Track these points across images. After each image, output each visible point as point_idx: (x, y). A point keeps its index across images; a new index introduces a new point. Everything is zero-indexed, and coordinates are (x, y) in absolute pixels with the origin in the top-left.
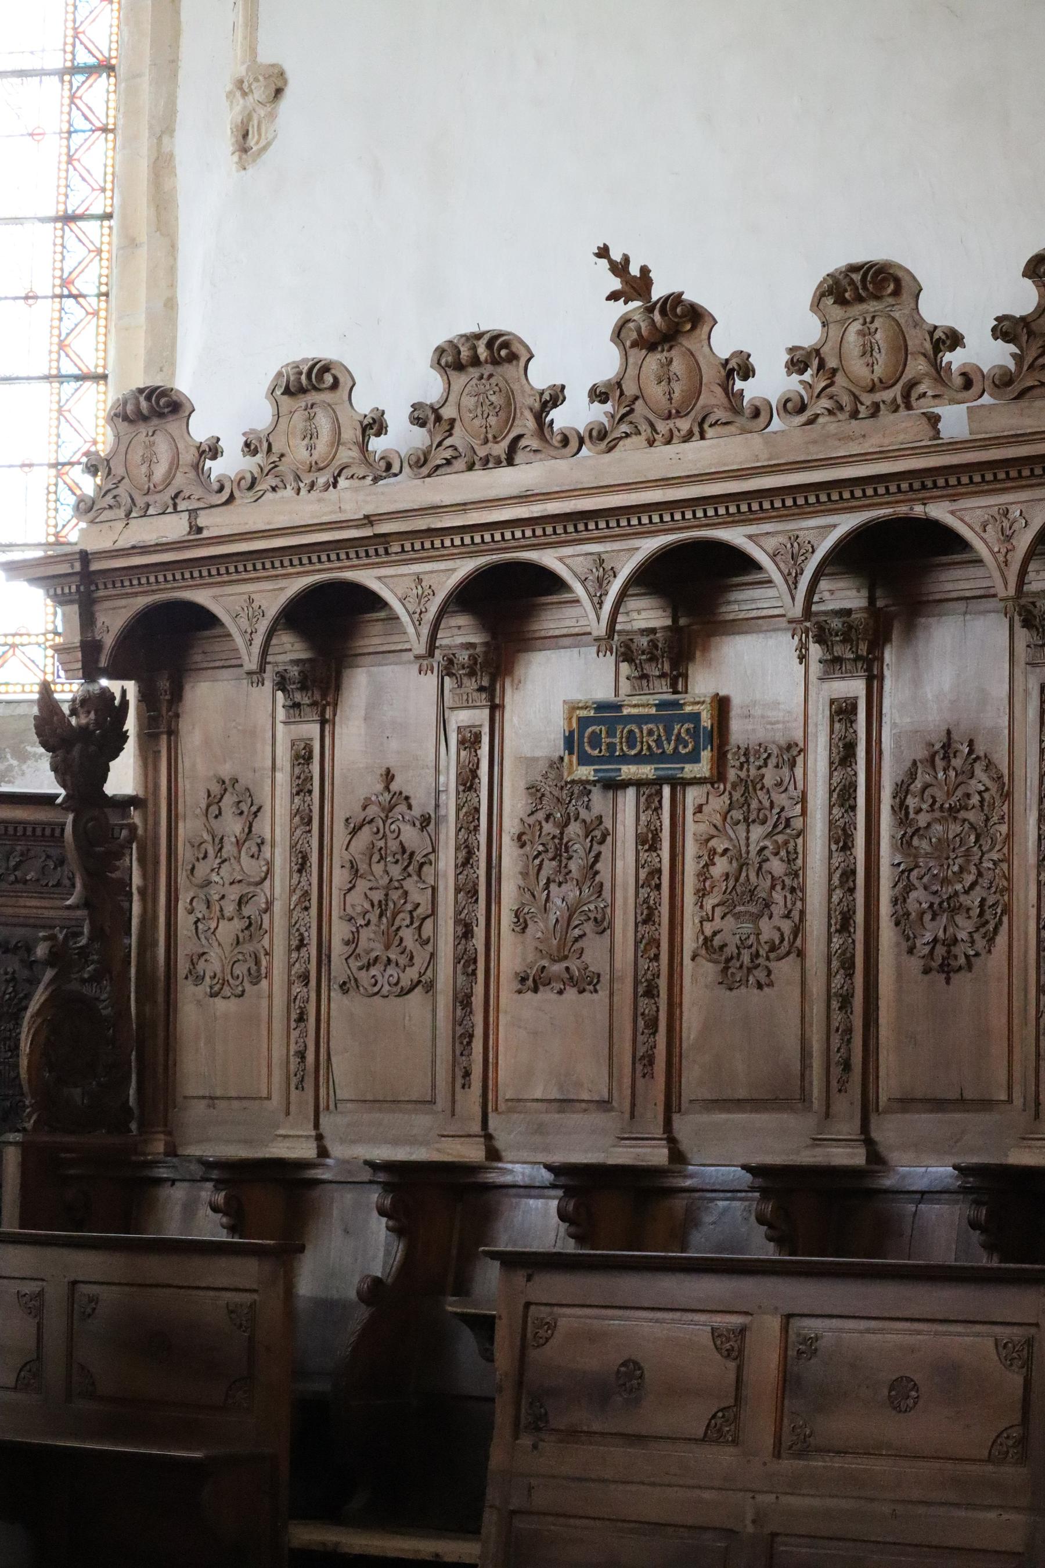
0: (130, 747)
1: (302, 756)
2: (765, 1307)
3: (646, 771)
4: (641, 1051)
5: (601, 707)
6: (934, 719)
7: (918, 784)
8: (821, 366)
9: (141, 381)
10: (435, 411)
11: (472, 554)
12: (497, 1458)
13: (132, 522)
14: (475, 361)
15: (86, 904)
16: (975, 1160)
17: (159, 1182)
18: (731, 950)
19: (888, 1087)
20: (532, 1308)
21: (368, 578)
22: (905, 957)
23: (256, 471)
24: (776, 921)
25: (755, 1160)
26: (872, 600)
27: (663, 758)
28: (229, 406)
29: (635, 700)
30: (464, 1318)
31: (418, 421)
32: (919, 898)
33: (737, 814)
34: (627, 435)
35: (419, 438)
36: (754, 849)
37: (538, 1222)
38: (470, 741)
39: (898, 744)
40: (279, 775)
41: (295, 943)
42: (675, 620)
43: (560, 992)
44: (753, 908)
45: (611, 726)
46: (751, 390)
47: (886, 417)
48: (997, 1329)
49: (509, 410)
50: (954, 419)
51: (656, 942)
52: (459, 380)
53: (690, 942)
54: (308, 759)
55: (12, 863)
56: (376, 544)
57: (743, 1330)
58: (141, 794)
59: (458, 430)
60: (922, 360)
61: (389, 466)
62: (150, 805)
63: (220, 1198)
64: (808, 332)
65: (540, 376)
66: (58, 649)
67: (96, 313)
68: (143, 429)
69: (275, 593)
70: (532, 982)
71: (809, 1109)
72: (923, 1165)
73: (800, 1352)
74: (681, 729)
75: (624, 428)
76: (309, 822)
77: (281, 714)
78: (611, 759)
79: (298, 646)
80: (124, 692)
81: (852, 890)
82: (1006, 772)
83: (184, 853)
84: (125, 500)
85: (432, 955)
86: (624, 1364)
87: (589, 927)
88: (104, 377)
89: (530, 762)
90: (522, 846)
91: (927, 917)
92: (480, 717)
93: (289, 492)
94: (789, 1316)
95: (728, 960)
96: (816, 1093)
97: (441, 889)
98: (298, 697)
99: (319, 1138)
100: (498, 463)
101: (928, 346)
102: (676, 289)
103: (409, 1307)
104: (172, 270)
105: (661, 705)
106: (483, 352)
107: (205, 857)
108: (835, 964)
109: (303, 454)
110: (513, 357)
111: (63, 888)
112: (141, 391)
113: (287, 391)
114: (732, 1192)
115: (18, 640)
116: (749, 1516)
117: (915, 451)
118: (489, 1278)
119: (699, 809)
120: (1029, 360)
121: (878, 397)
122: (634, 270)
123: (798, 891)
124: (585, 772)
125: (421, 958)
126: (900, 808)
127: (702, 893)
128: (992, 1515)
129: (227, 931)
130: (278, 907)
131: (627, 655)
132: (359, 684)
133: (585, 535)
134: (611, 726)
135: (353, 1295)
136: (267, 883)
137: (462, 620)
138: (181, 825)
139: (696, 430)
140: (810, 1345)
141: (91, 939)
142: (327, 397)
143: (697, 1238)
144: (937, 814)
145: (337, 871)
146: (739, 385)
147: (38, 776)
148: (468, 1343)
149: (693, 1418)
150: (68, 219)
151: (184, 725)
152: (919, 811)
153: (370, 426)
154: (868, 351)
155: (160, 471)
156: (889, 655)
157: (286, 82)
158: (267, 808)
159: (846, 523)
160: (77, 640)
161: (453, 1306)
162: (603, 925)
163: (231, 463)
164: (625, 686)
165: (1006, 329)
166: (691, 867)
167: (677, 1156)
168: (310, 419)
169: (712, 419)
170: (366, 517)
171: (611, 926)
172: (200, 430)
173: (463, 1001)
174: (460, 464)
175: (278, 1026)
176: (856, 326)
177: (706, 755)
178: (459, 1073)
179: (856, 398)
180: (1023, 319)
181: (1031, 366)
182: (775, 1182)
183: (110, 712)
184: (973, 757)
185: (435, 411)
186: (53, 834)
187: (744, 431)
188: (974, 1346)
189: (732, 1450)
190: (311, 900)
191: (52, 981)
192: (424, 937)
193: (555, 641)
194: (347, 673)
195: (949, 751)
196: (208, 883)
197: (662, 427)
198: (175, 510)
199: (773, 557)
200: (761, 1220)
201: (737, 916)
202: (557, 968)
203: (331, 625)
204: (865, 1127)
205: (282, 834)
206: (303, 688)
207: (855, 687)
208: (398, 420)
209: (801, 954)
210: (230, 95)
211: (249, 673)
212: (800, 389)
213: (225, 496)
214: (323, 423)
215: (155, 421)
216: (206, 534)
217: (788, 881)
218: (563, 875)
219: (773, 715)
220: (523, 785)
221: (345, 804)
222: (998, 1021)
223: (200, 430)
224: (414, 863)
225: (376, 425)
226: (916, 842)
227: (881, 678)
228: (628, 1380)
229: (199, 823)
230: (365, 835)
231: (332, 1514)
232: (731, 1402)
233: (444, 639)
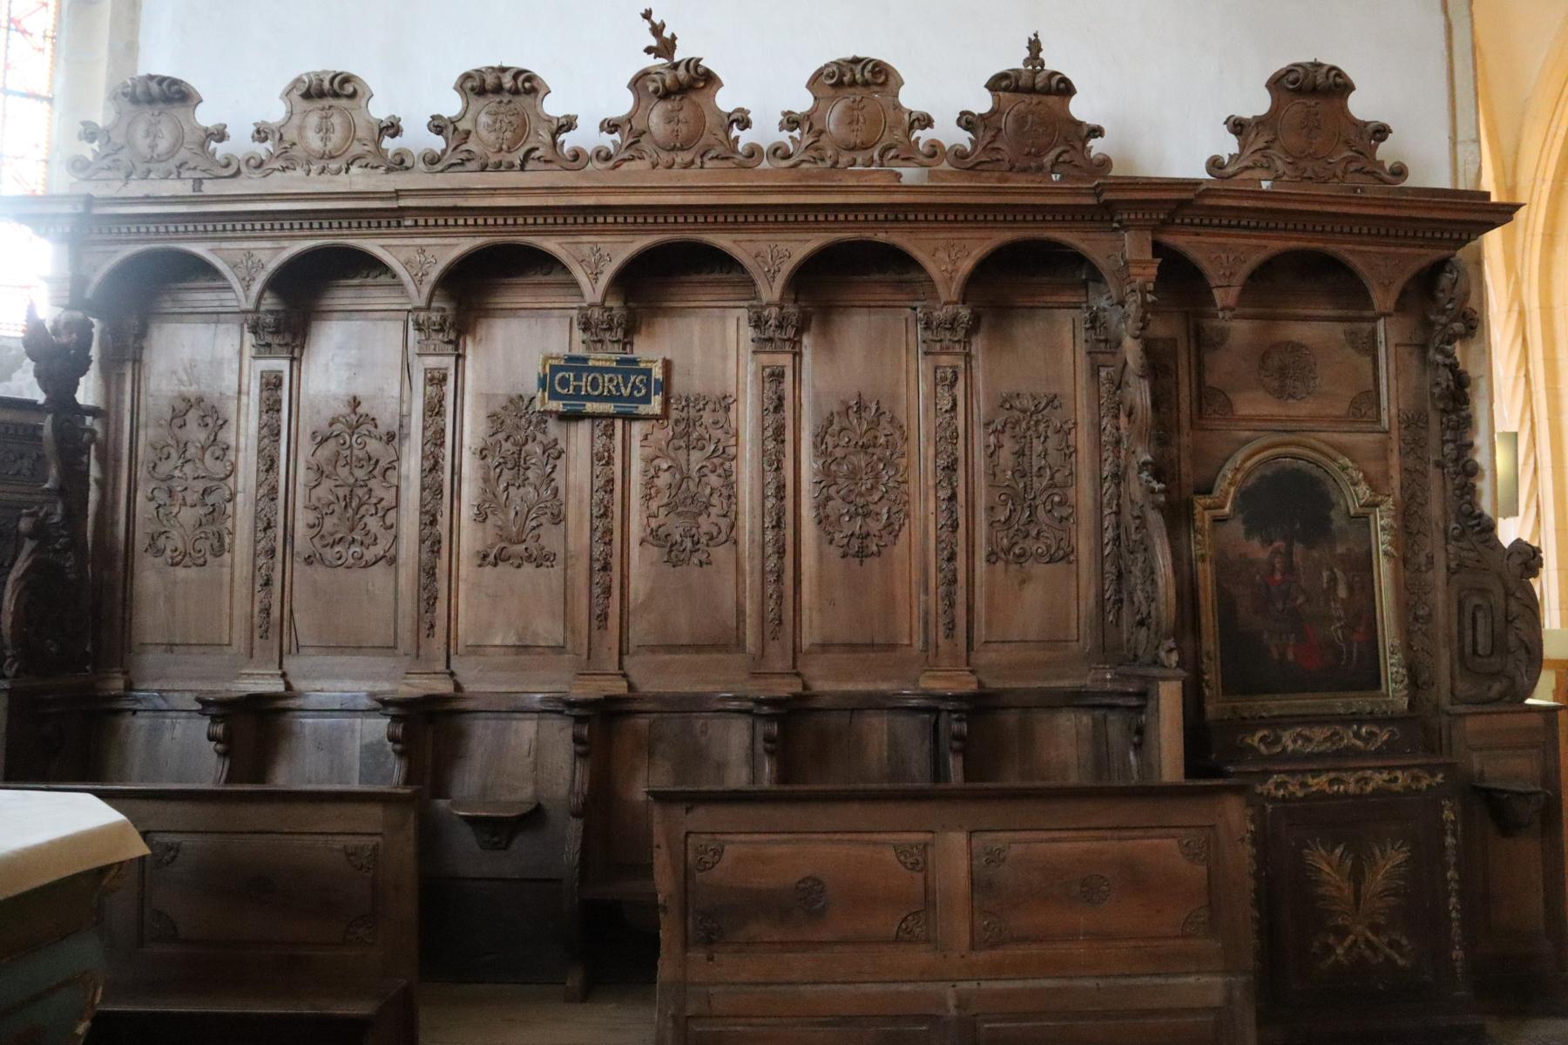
0: (94, 370)
3: (609, 408)
5: (570, 359)
7: (835, 427)
11: (474, 235)
14: (498, 89)
17: (121, 712)
22: (826, 546)
24: (713, 518)
27: (620, 398)
32: (836, 505)
43: (519, 566)
49: (521, 129)
52: (478, 103)
54: (278, 385)
58: (102, 406)
62: (112, 415)
68: (148, 112)
76: (278, 434)
77: (248, 351)
78: (577, 395)
90: (484, 458)
108: (769, 550)
116: (951, 1003)
123: (732, 497)
127: (647, 498)
128: (1192, 980)
129: (188, 516)
136: (231, 479)
138: (142, 433)
139: (698, 161)
142: (344, 102)
153: (387, 128)
162: (558, 518)
163: (240, 143)
165: (967, 121)
170: (397, 191)
180: (981, 115)
191: (33, 551)
192: (388, 523)
194: (314, 324)
198: (179, 177)
201: (679, 514)
206: (277, 332)
213: (232, 170)
215: (161, 105)
220: (483, 414)
226: (833, 467)
230: (331, 445)
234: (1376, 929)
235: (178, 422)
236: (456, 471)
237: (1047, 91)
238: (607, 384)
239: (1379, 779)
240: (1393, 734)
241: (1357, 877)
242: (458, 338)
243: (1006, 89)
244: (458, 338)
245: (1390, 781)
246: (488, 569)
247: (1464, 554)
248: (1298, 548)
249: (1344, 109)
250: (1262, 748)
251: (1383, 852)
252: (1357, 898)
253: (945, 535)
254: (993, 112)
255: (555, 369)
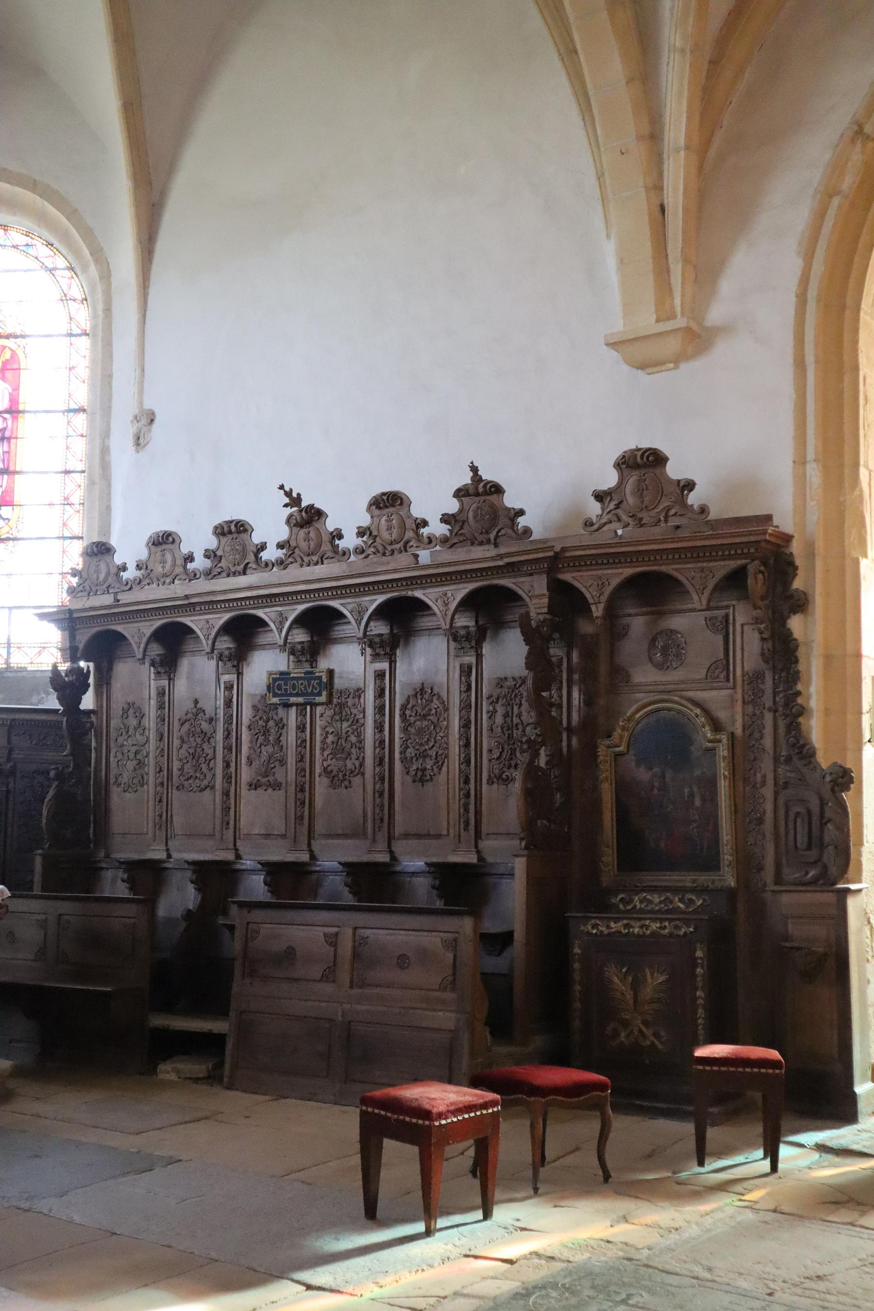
0: (91, 690)
1: (161, 693)
2: (348, 925)
3: (300, 700)
4: (299, 814)
5: (282, 673)
6: (417, 679)
7: (410, 706)
8: (371, 534)
9: (95, 539)
10: (214, 552)
12: (235, 988)
13: (91, 598)
14: (230, 532)
15: (72, 754)
16: (435, 860)
18: (335, 773)
19: (398, 830)
20: (250, 925)
21: (187, 621)
23: (141, 577)
24: (353, 760)
25: (342, 860)
26: (391, 630)
27: (307, 694)
28: (130, 551)
29: (296, 671)
30: (225, 925)
31: (207, 556)
32: (410, 752)
33: (337, 717)
34: (292, 563)
35: (208, 563)
36: (344, 731)
37: (256, 886)
38: (229, 687)
39: (402, 689)
40: (152, 701)
41: (158, 770)
42: (312, 638)
44: (343, 756)
45: (286, 680)
46: (342, 544)
47: (397, 555)
48: (442, 934)
49: (244, 552)
50: (425, 556)
51: (304, 770)
52: (224, 540)
53: (318, 770)
55: (42, 737)
56: (190, 606)
57: (337, 934)
59: (223, 560)
60: (411, 532)
61: (195, 575)
63: (125, 876)
64: (365, 520)
65: (257, 538)
66: (61, 650)
67: (78, 511)
68: (95, 559)
69: (149, 627)
70: (254, 786)
71: (367, 838)
72: (413, 862)
73: (360, 944)
74: (315, 683)
75: (291, 560)
76: (164, 720)
77: (153, 676)
78: (286, 695)
79: (160, 648)
80: (88, 667)
81: (384, 748)
82: (445, 699)
83: (113, 734)
84: (88, 588)
85: (214, 775)
86: (288, 948)
87: (277, 763)
88: (82, 538)
89: (253, 696)
91: (414, 759)
92: (233, 677)
93: (155, 585)
94: (355, 929)
95: (334, 777)
96: (369, 831)
97: (217, 748)
98: (159, 669)
99: (168, 850)
100: (240, 574)
101: (414, 526)
102: (312, 503)
103: (203, 923)
104: (109, 494)
105: (306, 673)
106: (233, 528)
107: (122, 734)
108: (377, 778)
109: (160, 569)
110: (245, 530)
111: (63, 747)
112: (94, 543)
113: (153, 544)
114: (335, 872)
115: (46, 645)
116: (340, 1013)
117: (408, 569)
118: (234, 910)
119: (322, 715)
120: (455, 531)
121: (393, 547)
122: (294, 495)
123: (362, 749)
124: (275, 700)
125: (209, 776)
126: (403, 716)
127: (323, 749)
128: (441, 1014)
129: (131, 765)
130: (151, 755)
131: (292, 652)
132: (185, 664)
133: (275, 603)
134: (286, 680)
135: (179, 916)
137: (225, 638)
140: (365, 940)
141: (74, 769)
142: (169, 546)
143: (321, 891)
144: (418, 717)
145: (175, 740)
146: (337, 542)
147: (52, 702)
148: (227, 933)
149: (316, 972)
150: (67, 472)
151: (113, 682)
152: (411, 716)
153: (187, 559)
154: (389, 528)
155: (102, 576)
156: (398, 652)
157: (155, 417)
158: (147, 714)
159: (381, 599)
160: (68, 645)
161: (221, 921)
162: (283, 762)
163: (130, 574)
164: (292, 665)
165: (446, 519)
166: (318, 738)
167: (313, 857)
168: (163, 555)
169: (326, 556)
171: (286, 763)
172: (118, 560)
173: (226, 794)
174: (224, 574)
175: (151, 803)
176: (385, 518)
177: (324, 693)
178: (225, 823)
179: (385, 547)
181: (456, 534)
182: (352, 869)
183: (83, 676)
184: (432, 694)
185: (214, 552)
186: (57, 725)
187: (339, 561)
188: (433, 941)
189: (331, 985)
190: (165, 752)
191: (57, 786)
193: (263, 647)
195: (423, 692)
196: (123, 745)
197: (306, 559)
199: (351, 612)
200: (346, 885)
202: (264, 780)
203: (172, 641)
204: (389, 846)
205: (153, 725)
206: (162, 665)
207: (385, 665)
208: (199, 557)
209: (363, 774)
210: (132, 422)
211: (139, 660)
212: (362, 544)
213: (128, 587)
214: (169, 557)
215: (100, 556)
216: (121, 602)
217: (358, 745)
218: (267, 742)
219: (351, 677)
220: (250, 706)
221: (178, 713)
222: (443, 801)
223: (118, 560)
224: (207, 737)
225: (190, 558)
226: (409, 729)
227: (395, 662)
228: (290, 954)
229: (120, 721)
230: (187, 726)
231: (168, 1008)
232: (331, 965)
233: (218, 645)
234: (646, 1023)
235: (125, 716)
236: (238, 738)
237: (486, 493)
238: (301, 685)
239: (655, 926)
240: (704, 900)
241: (636, 986)
242: (238, 663)
243: (463, 496)
244: (238, 663)
245: (661, 928)
246: (253, 792)
247: (788, 774)
248: (669, 774)
249: (664, 473)
250: (621, 906)
251: (652, 974)
252: (635, 1001)
253: (463, 767)
254: (461, 511)
255: (275, 680)
